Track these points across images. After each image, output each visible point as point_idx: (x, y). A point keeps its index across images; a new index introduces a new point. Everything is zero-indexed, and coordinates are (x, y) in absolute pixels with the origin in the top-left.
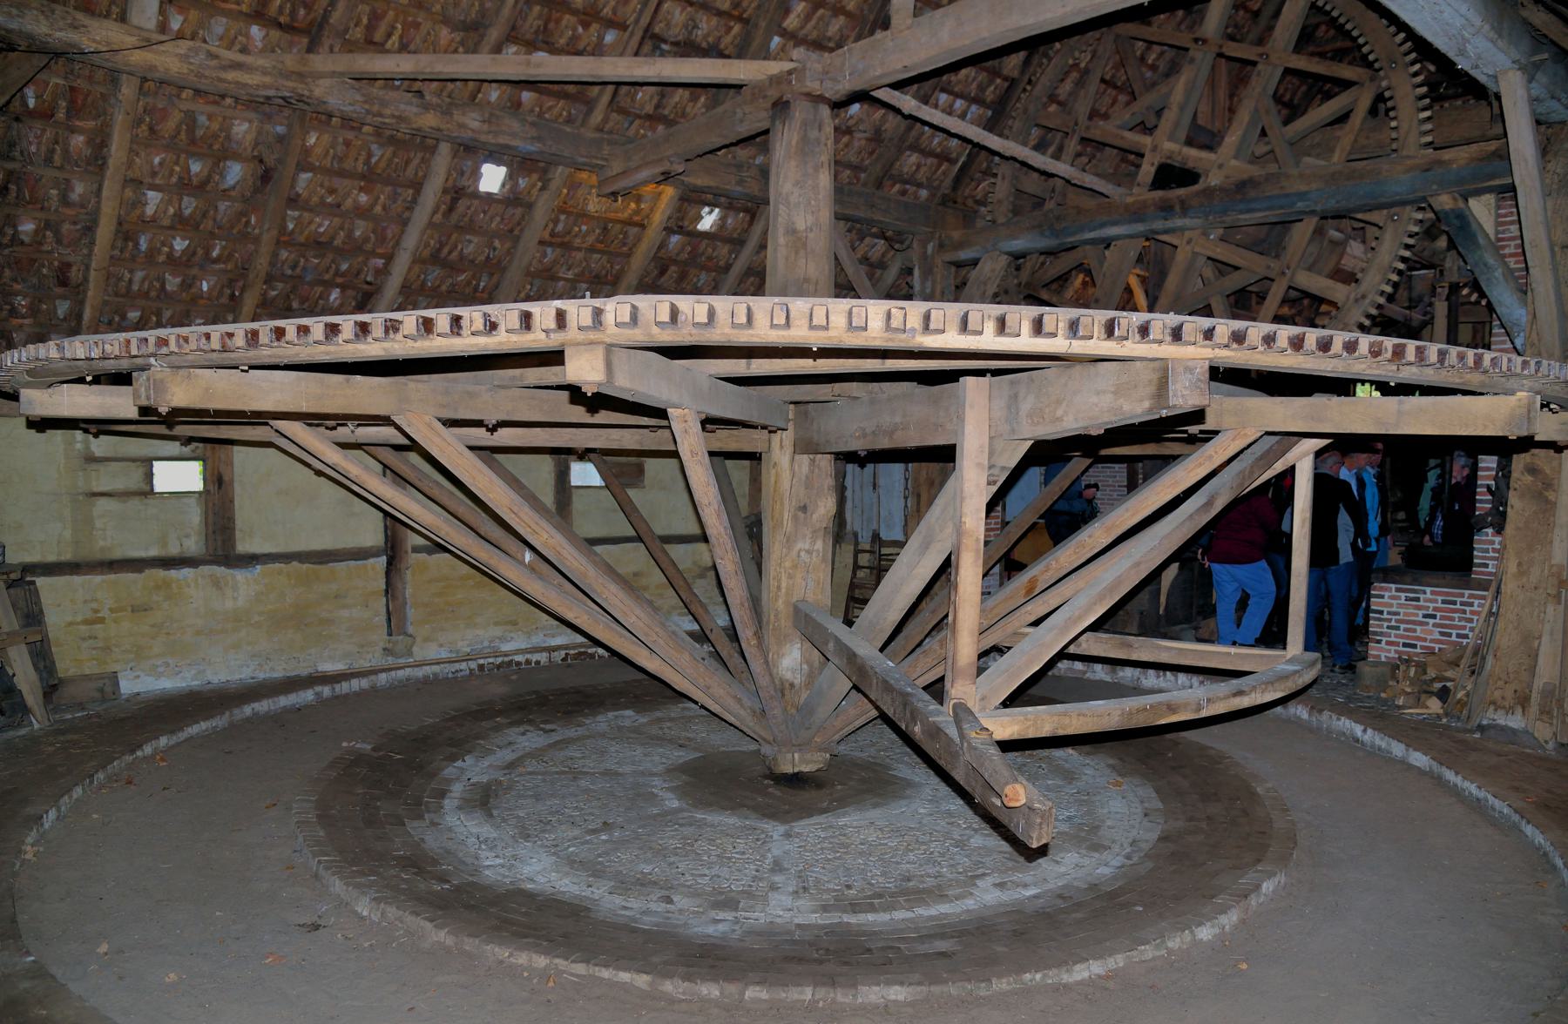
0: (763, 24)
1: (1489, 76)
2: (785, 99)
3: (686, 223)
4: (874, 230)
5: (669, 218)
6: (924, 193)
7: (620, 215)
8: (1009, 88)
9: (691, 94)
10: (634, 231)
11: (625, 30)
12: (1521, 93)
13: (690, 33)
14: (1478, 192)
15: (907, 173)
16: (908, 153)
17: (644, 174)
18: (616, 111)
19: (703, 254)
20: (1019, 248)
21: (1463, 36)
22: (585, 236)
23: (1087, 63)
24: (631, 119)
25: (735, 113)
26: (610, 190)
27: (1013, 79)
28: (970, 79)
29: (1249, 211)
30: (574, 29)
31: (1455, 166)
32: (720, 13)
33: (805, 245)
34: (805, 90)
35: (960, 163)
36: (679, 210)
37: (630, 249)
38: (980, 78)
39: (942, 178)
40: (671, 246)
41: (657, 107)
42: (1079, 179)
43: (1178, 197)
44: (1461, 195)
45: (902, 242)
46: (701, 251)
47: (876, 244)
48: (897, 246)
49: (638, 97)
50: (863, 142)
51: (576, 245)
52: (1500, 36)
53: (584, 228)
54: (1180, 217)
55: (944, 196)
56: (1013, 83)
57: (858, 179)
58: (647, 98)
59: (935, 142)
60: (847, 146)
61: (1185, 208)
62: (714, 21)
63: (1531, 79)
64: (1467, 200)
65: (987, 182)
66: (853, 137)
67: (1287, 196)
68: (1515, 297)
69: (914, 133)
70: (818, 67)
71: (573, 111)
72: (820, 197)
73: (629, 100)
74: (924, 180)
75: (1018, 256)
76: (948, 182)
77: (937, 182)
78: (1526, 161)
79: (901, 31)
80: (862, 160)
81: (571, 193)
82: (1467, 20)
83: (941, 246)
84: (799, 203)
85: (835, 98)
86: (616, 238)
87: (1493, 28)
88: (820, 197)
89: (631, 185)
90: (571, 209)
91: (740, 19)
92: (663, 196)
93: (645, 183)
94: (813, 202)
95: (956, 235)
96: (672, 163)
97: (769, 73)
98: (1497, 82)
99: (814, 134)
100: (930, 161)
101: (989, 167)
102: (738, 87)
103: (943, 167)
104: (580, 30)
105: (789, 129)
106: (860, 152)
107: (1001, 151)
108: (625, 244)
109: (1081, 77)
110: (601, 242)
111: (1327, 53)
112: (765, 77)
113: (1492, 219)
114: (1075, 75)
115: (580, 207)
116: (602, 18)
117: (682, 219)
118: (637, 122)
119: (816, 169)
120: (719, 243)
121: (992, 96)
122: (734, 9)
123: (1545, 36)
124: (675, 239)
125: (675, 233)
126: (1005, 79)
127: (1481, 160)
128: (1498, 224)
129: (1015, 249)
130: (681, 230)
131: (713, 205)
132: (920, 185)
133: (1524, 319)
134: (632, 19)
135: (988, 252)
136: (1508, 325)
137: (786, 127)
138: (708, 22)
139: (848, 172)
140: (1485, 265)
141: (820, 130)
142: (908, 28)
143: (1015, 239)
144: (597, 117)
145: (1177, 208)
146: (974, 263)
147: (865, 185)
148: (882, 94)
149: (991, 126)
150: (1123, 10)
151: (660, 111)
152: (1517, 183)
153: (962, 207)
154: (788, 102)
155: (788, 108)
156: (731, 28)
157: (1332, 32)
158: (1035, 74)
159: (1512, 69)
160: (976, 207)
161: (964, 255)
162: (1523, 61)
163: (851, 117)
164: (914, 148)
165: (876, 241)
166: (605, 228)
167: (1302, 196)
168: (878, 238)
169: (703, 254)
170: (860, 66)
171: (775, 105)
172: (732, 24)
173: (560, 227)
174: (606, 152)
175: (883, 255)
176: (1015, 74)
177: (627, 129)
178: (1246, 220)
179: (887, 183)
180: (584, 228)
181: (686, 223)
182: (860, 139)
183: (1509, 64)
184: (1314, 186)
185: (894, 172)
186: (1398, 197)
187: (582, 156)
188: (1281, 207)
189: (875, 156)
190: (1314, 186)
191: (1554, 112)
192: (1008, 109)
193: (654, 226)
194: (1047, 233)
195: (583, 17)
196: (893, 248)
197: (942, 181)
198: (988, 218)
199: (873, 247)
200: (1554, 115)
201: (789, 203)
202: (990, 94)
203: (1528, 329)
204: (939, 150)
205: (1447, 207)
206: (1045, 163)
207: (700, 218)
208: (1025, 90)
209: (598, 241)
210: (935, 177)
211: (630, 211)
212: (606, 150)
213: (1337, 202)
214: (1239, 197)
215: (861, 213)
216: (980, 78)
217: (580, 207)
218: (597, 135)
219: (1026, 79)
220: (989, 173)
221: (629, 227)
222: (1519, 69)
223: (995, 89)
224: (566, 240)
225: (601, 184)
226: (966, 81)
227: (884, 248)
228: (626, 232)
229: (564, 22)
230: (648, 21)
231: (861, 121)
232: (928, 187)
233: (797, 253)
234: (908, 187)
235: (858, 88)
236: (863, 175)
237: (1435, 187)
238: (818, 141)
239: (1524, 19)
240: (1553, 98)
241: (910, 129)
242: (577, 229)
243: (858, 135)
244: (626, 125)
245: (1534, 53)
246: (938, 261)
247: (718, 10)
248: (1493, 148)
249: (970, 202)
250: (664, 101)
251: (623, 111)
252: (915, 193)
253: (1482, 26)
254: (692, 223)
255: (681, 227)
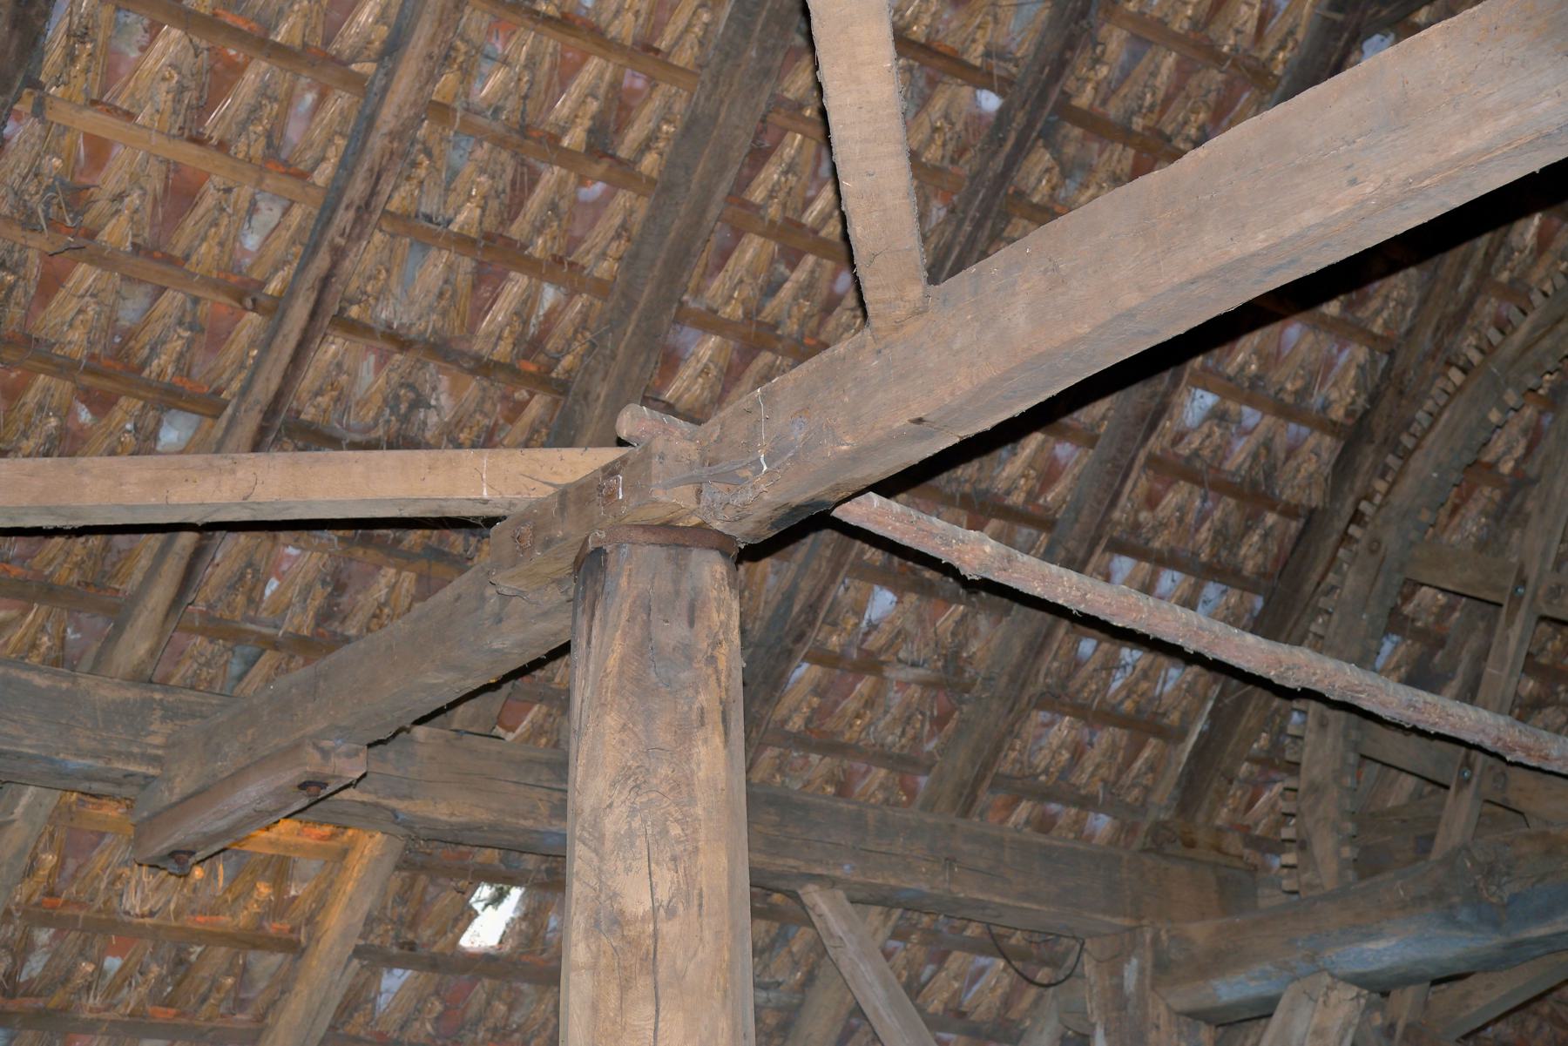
0: (602, 390)
2: (590, 547)
3: (425, 934)
4: (973, 930)
5: (370, 921)
6: (1101, 824)
7: (225, 919)
8: (1302, 533)
9: (421, 578)
10: (267, 963)
11: (216, 417)
13: (405, 419)
15: (1046, 771)
16: (1042, 716)
17: (253, 793)
18: (202, 631)
19: (480, 1019)
20: (1387, 961)
22: (115, 989)
23: (1517, 462)
24: (249, 650)
25: (483, 599)
26: (165, 845)
28: (1191, 518)
30: (66, 413)
32: (484, 368)
33: (651, 961)
34: (656, 514)
35: (1192, 739)
36: (402, 898)
37: (260, 1019)
38: (1217, 514)
39: (1148, 780)
40: (382, 1001)
41: (324, 616)
42: (1527, 750)
45: (1055, 963)
46: (472, 1012)
47: (981, 971)
48: (1043, 975)
49: (268, 592)
50: (915, 692)
51: (86, 1015)
53: (113, 963)
55: (1159, 826)
56: (1312, 520)
57: (911, 793)
58: (293, 593)
59: (1116, 685)
60: (869, 703)
62: (473, 387)
65: (1278, 788)
66: (883, 679)
69: (1050, 663)
70: (691, 450)
71: (71, 635)
72: (699, 811)
73: (240, 599)
74: (1098, 788)
75: (1380, 987)
76: (1165, 792)
77: (1136, 792)
79: (898, 326)
80: (916, 739)
81: (71, 865)
83: (1162, 968)
84: (631, 833)
85: (745, 531)
86: (215, 985)
88: (699, 811)
89: (222, 824)
90: (68, 912)
91: (543, 381)
92: (354, 856)
93: (264, 818)
94: (675, 830)
95: (1200, 932)
96: (326, 754)
97: (558, 481)
99: (672, 632)
100: (1106, 737)
101: (1276, 746)
102: (478, 525)
103: (1146, 753)
104: (85, 416)
105: (603, 628)
106: (909, 720)
107: (1272, 674)
108: (241, 1004)
109: (1507, 498)
110: (169, 1003)
112: (551, 490)
114: (1487, 494)
115: (99, 903)
116: (148, 385)
117: (413, 924)
118: (269, 659)
119: (684, 733)
120: (525, 987)
122: (526, 357)
124: (394, 981)
125: (392, 962)
126: (1289, 512)
129: (1376, 967)
130: (409, 954)
131: (503, 880)
132: (1086, 803)
134: (236, 386)
135: (1296, 979)
137: (596, 622)
138: (454, 392)
139: (882, 772)
141: (691, 623)
142: (918, 312)
143: (1369, 936)
144: (136, 645)
146: (1264, 1010)
147: (929, 805)
148: (871, 512)
149: (1269, 626)
151: (335, 626)
154: (599, 551)
155: (602, 568)
156: (521, 407)
158: (1368, 498)
161: (1230, 989)
163: (873, 627)
164: (1056, 700)
165: (983, 961)
166: (180, 961)
168: (983, 952)
169: (480, 1019)
170: (798, 435)
171: (578, 565)
172: (521, 394)
173: (35, 966)
174: (158, 740)
175: (1007, 1002)
176: (1316, 498)
177: (240, 678)
179: (984, 797)
180: (113, 963)
181: (425, 934)
182: (904, 685)
185: (1005, 766)
187: (80, 753)
189: (950, 726)
192: (1308, 588)
193: (324, 946)
194: (1464, 915)
195: (88, 380)
196: (1031, 982)
197: (1148, 790)
198: (1287, 884)
199: (975, 979)
201: (601, 838)
202: (1251, 554)
204: (1128, 706)
206: (1411, 705)
207: (467, 916)
208: (1346, 538)
209: (155, 996)
210: (1127, 779)
211: (255, 908)
212: (158, 734)
215: (919, 882)
216: (1217, 514)
217: (99, 903)
218: (132, 694)
219: (1347, 510)
220: (1277, 763)
221: (252, 955)
223: (1265, 536)
224: (55, 1001)
225: (143, 830)
226: (1181, 520)
227: (1006, 981)
228: (245, 968)
229: (31, 398)
230: (274, 386)
231: (900, 635)
232: (1112, 805)
233: (624, 987)
234: (1054, 807)
235: (799, 499)
236: (923, 781)
238: (686, 652)
241: (1037, 647)
242: (88, 967)
243: (895, 674)
244: (236, 668)
246: (1159, 1010)
247: (478, 358)
249: (1233, 843)
250: (345, 599)
251: (215, 628)
252: (1078, 823)
254: (442, 932)
255: (411, 946)
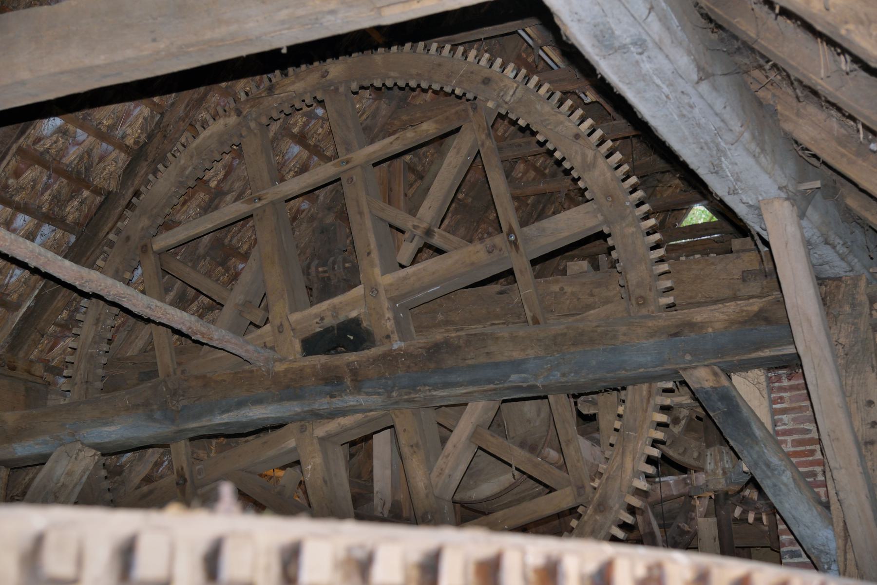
1: (750, 206)
8: (102, 204)
12: (792, 229)
14: (745, 366)
20: (114, 437)
21: (717, 145)
27: (110, 193)
28: (39, 187)
29: (446, 385)
31: (710, 330)
42: (203, 334)
43: (348, 365)
44: (723, 370)
52: (763, 150)
54: (351, 394)
56: (109, 197)
61: (358, 381)
63: (802, 215)
64: (730, 377)
67: (497, 365)
68: (815, 512)
78: (809, 321)
82: (723, 121)
87: (754, 137)
98: (760, 215)
107: (77, 284)
109: (212, 200)
111: (528, 197)
113: (766, 403)
114: (202, 196)
121: (77, 214)
123: (815, 156)
126: (97, 191)
127: (744, 323)
128: (774, 412)
133: (833, 545)
136: (813, 553)
140: (768, 465)
143: (106, 424)
145: (348, 381)
146: (41, 461)
150: (249, 57)
152: (801, 351)
153: (26, 376)
157: (532, 174)
159: (779, 198)
160: (49, 377)
161: (22, 449)
162: (791, 188)
167: (517, 365)
176: (113, 186)
178: (442, 397)
183: (774, 191)
184: (531, 353)
186: (642, 370)
188: (489, 381)
190: (531, 353)
191: (827, 263)
194: (158, 415)
200: (827, 267)
202: (72, 211)
203: (841, 559)
205: (707, 385)
206: (149, 307)
213: (564, 375)
214: (432, 366)
222: (787, 199)
226: (33, 187)
237: (688, 357)
239: (786, 133)
240: (827, 243)
245: (802, 179)
248: (756, 308)
249: (38, 369)
253: (742, 134)
